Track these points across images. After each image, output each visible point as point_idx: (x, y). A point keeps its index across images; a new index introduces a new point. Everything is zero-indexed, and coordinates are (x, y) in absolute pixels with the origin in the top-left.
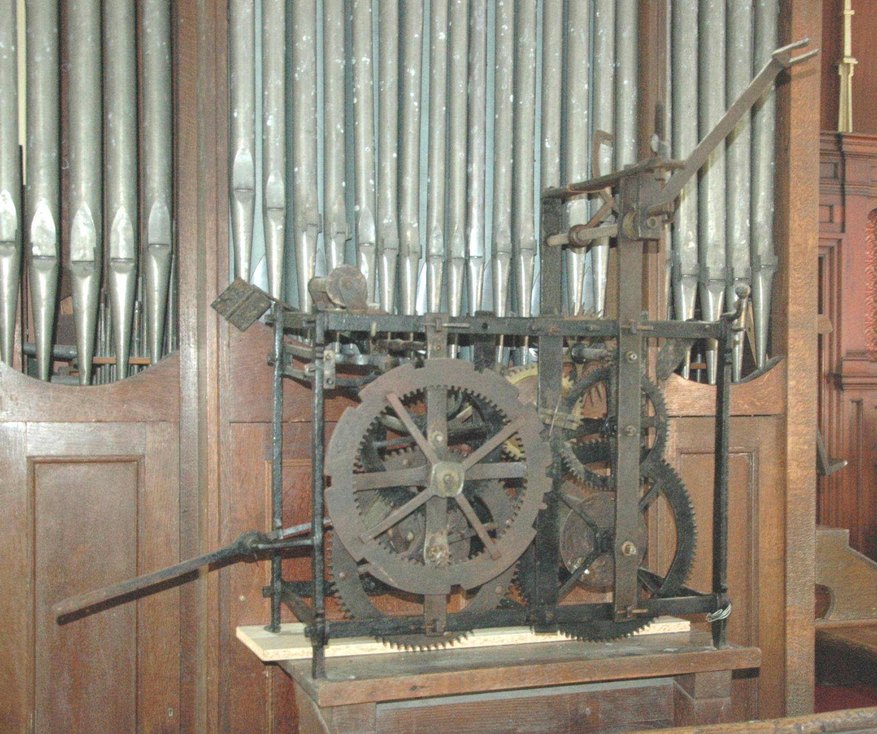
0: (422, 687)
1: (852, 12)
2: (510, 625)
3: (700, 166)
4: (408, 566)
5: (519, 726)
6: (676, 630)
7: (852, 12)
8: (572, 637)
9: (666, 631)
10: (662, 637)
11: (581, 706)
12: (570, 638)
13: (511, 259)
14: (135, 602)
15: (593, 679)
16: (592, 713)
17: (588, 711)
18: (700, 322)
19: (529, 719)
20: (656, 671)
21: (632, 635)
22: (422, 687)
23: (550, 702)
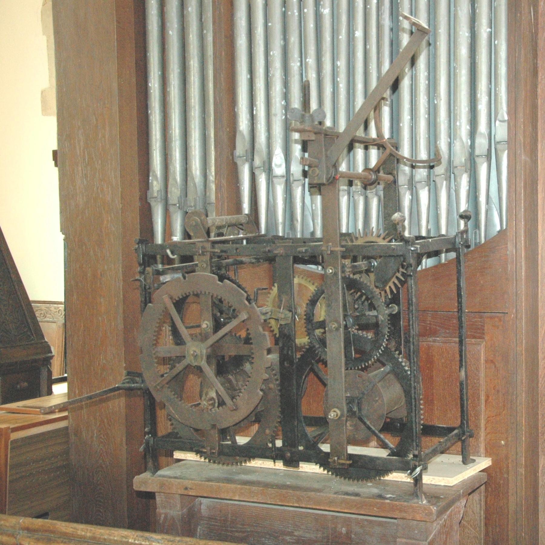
0: (191, 489)
1: (177, 365)
2: (262, 458)
3: (365, 119)
4: (14, 540)
5: (296, 530)
6: (442, 484)
7: (177, 365)
8: (328, 472)
9: (433, 483)
10: (434, 487)
11: (339, 526)
12: (326, 472)
13: (253, 160)
14: (40, 324)
15: (301, 506)
16: (347, 533)
17: (344, 530)
18: (355, 264)
19: (302, 527)
20: (347, 508)
21: (380, 479)
22: (191, 489)
23: (317, 518)
